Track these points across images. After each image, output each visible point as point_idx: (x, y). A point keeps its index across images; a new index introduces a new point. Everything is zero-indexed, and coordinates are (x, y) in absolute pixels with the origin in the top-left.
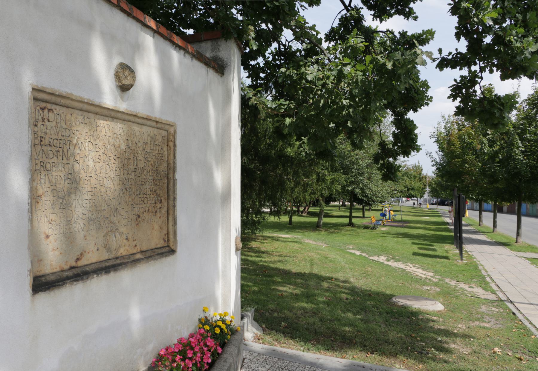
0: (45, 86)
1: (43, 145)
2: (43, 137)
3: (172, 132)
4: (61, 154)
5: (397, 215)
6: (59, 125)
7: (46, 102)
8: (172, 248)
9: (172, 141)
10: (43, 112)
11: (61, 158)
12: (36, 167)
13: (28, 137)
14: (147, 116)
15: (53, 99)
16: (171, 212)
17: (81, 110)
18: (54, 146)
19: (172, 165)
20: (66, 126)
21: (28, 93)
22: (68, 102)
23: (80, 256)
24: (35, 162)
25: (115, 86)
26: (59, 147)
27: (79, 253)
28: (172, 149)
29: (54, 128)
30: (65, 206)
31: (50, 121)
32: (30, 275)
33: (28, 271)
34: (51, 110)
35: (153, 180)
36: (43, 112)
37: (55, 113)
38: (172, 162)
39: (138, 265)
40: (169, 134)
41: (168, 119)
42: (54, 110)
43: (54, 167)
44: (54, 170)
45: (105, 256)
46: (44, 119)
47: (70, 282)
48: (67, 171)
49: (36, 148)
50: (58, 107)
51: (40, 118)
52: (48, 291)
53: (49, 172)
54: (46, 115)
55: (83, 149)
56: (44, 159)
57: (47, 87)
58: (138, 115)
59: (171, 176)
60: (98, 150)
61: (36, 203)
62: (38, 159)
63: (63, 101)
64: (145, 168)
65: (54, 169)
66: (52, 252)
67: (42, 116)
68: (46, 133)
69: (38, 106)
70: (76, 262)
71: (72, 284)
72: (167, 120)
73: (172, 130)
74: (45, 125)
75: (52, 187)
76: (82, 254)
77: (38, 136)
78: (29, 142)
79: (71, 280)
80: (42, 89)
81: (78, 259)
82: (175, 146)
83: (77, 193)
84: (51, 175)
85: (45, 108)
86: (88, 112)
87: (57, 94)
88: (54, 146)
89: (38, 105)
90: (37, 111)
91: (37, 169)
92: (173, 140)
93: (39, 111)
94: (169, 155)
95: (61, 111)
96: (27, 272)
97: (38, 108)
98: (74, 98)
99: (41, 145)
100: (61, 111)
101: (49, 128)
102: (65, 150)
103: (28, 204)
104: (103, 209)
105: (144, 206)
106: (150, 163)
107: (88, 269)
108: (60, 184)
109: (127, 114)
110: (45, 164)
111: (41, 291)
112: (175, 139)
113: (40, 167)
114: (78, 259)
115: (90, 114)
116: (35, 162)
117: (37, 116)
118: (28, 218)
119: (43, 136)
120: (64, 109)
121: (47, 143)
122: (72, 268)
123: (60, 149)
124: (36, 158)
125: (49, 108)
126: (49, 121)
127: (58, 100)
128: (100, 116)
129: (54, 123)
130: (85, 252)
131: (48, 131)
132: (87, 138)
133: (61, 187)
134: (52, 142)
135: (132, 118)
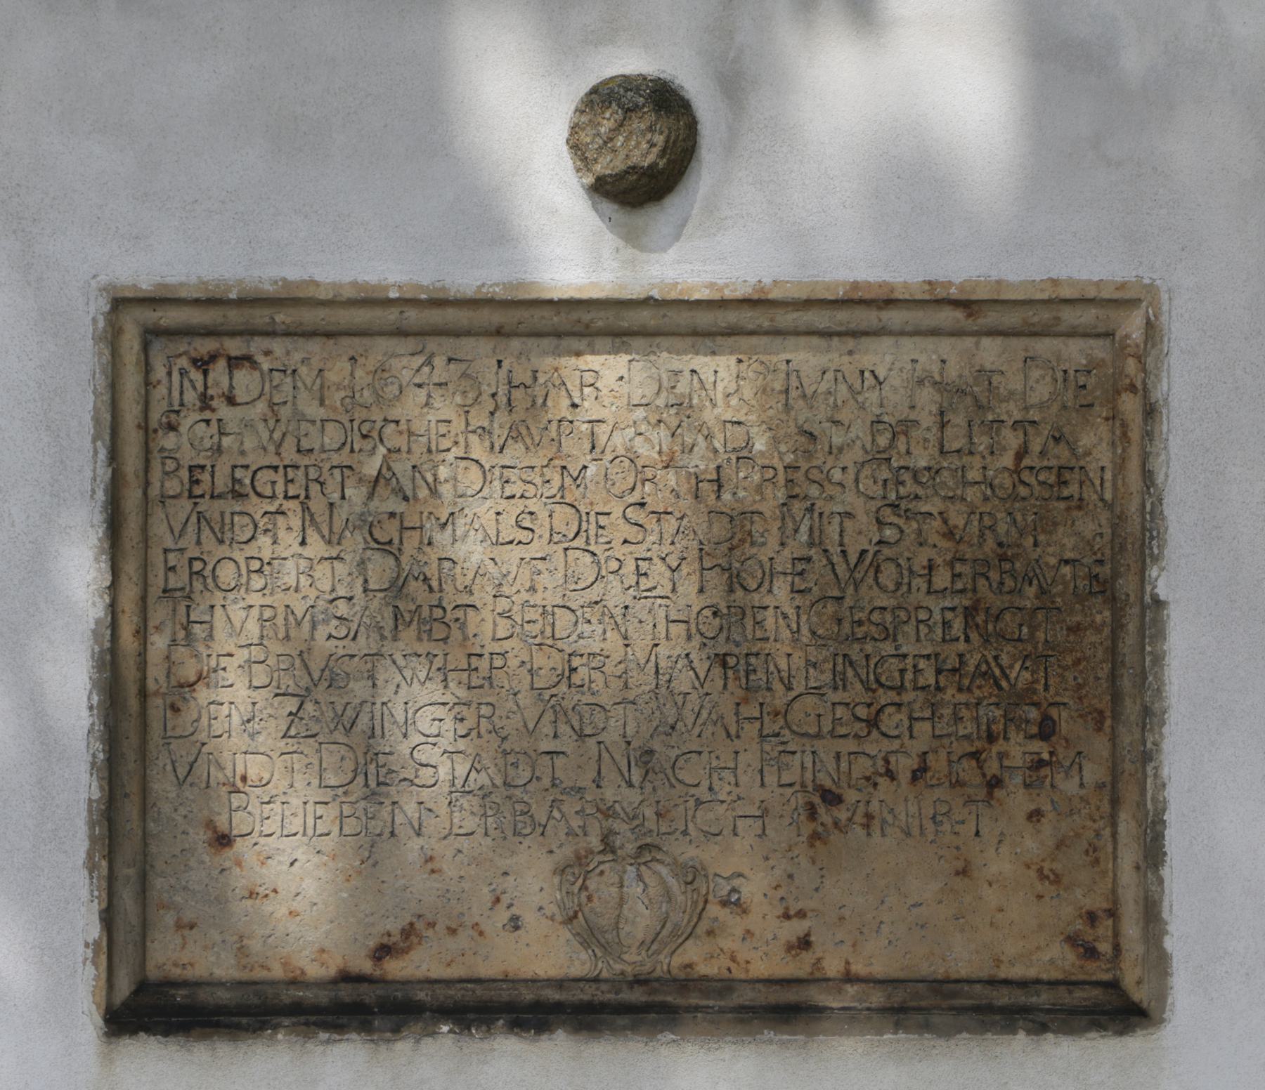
0: (170, 280)
1: (202, 496)
2: (203, 467)
4: (296, 522)
6: (285, 412)
10: (205, 373)
12: (166, 580)
13: (89, 474)
15: (234, 317)
19: (1134, 525)
20: (322, 410)
21: (94, 320)
22: (310, 317)
24: (166, 561)
25: (581, 191)
26: (286, 497)
28: (1135, 434)
31: (239, 400)
32: (95, 963)
33: (87, 945)
34: (248, 359)
36: (205, 373)
37: (266, 367)
39: (768, 1034)
41: (1061, 272)
42: (260, 358)
43: (253, 576)
45: (579, 963)
46: (212, 398)
47: (294, 1024)
49: (171, 511)
51: (191, 397)
52: (182, 1039)
53: (231, 596)
55: (423, 493)
56: (206, 547)
57: (183, 279)
58: (898, 295)
60: (516, 488)
62: (182, 550)
63: (283, 317)
64: (887, 552)
65: (257, 582)
67: (200, 388)
68: (218, 450)
69: (180, 355)
71: (308, 1036)
72: (1055, 282)
73: (1133, 327)
74: (214, 424)
75: (246, 651)
76: (409, 932)
77: (178, 467)
78: (93, 492)
79: (302, 1019)
80: (158, 294)
82: (1150, 412)
83: (381, 678)
84: (242, 604)
85: (213, 358)
86: (457, 333)
87: (233, 295)
88: (259, 495)
89: (182, 350)
92: (1139, 385)
93: (183, 373)
96: (81, 949)
97: (184, 362)
99: (191, 496)
101: (231, 427)
103: (91, 708)
104: (545, 746)
107: (422, 995)
109: (723, 304)
110: (210, 567)
111: (150, 1030)
115: (467, 344)
116: (166, 561)
117: (176, 394)
118: (90, 759)
119: (202, 462)
120: (314, 346)
121: (222, 483)
122: (346, 977)
124: (169, 543)
126: (231, 401)
127: (260, 317)
128: (531, 342)
129: (261, 406)
130: (432, 925)
131: (226, 441)
132: (446, 443)
133: (295, 653)
134: (247, 481)
135: (747, 318)
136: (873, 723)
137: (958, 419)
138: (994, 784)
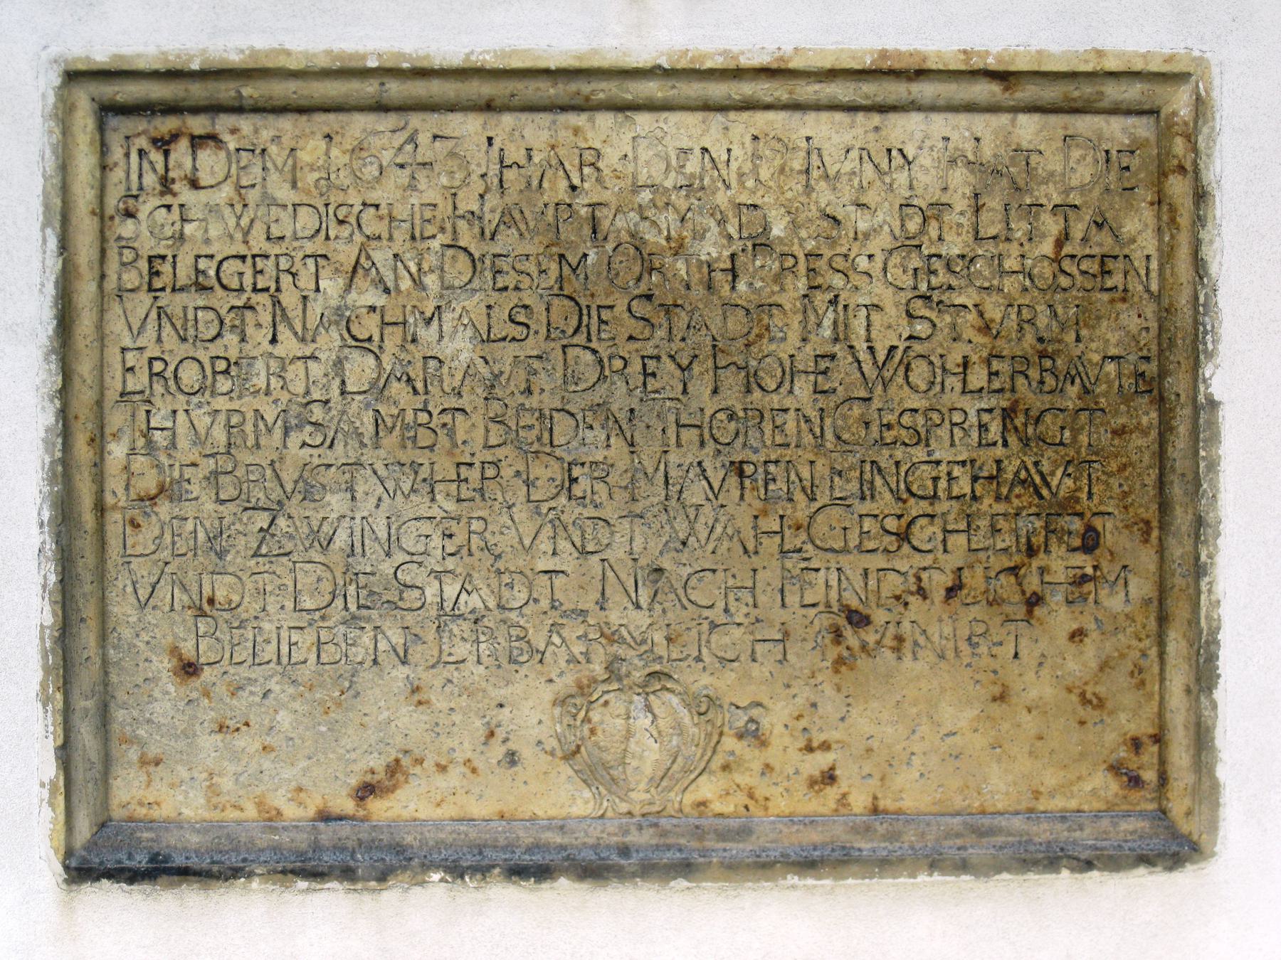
0: (126, 50)
2: (163, 257)
3: (1185, 112)
4: (266, 318)
5: (712, 436)
7: (171, 109)
8: (1185, 827)
9: (1181, 169)
10: (166, 154)
11: (264, 336)
14: (884, 54)
15: (198, 92)
16: (1180, 611)
17: (381, 108)
18: (224, 287)
19: (1184, 318)
23: (381, 775)
24: (124, 361)
27: (378, 763)
28: (1184, 220)
29: (227, 211)
30: (289, 546)
31: (203, 183)
32: (51, 804)
33: (42, 785)
35: (1007, 414)
36: (166, 154)
37: (232, 146)
38: (1183, 300)
40: (1166, 129)
42: (226, 137)
44: (225, 389)
46: (173, 181)
48: (300, 389)
49: (129, 305)
50: (246, 124)
54: (180, 166)
56: (167, 347)
59: (1177, 383)
61: (129, 530)
64: (918, 348)
66: (219, 737)
68: (181, 237)
70: (362, 799)
73: (1180, 103)
78: (43, 285)
80: (114, 66)
81: (366, 791)
82: (1201, 196)
87: (195, 66)
88: (224, 287)
90: (134, 157)
91: (130, 388)
92: (1188, 166)
93: (141, 153)
94: (1167, 254)
95: (266, 135)
97: (142, 142)
98: (293, 65)
99: (150, 289)
100: (266, 135)
102: (289, 298)
103: (42, 525)
104: (542, 565)
105: (907, 562)
106: (972, 317)
108: (258, 446)
112: (1195, 150)
113: (146, 380)
114: (366, 791)
116: (124, 361)
117: (134, 177)
119: (162, 252)
120: (286, 124)
121: (184, 273)
123: (263, 299)
124: (127, 342)
125: (198, 131)
126: (194, 184)
130: (419, 761)
131: (189, 229)
134: (212, 273)
136: (904, 536)
137: (994, 203)
138: (1034, 601)
